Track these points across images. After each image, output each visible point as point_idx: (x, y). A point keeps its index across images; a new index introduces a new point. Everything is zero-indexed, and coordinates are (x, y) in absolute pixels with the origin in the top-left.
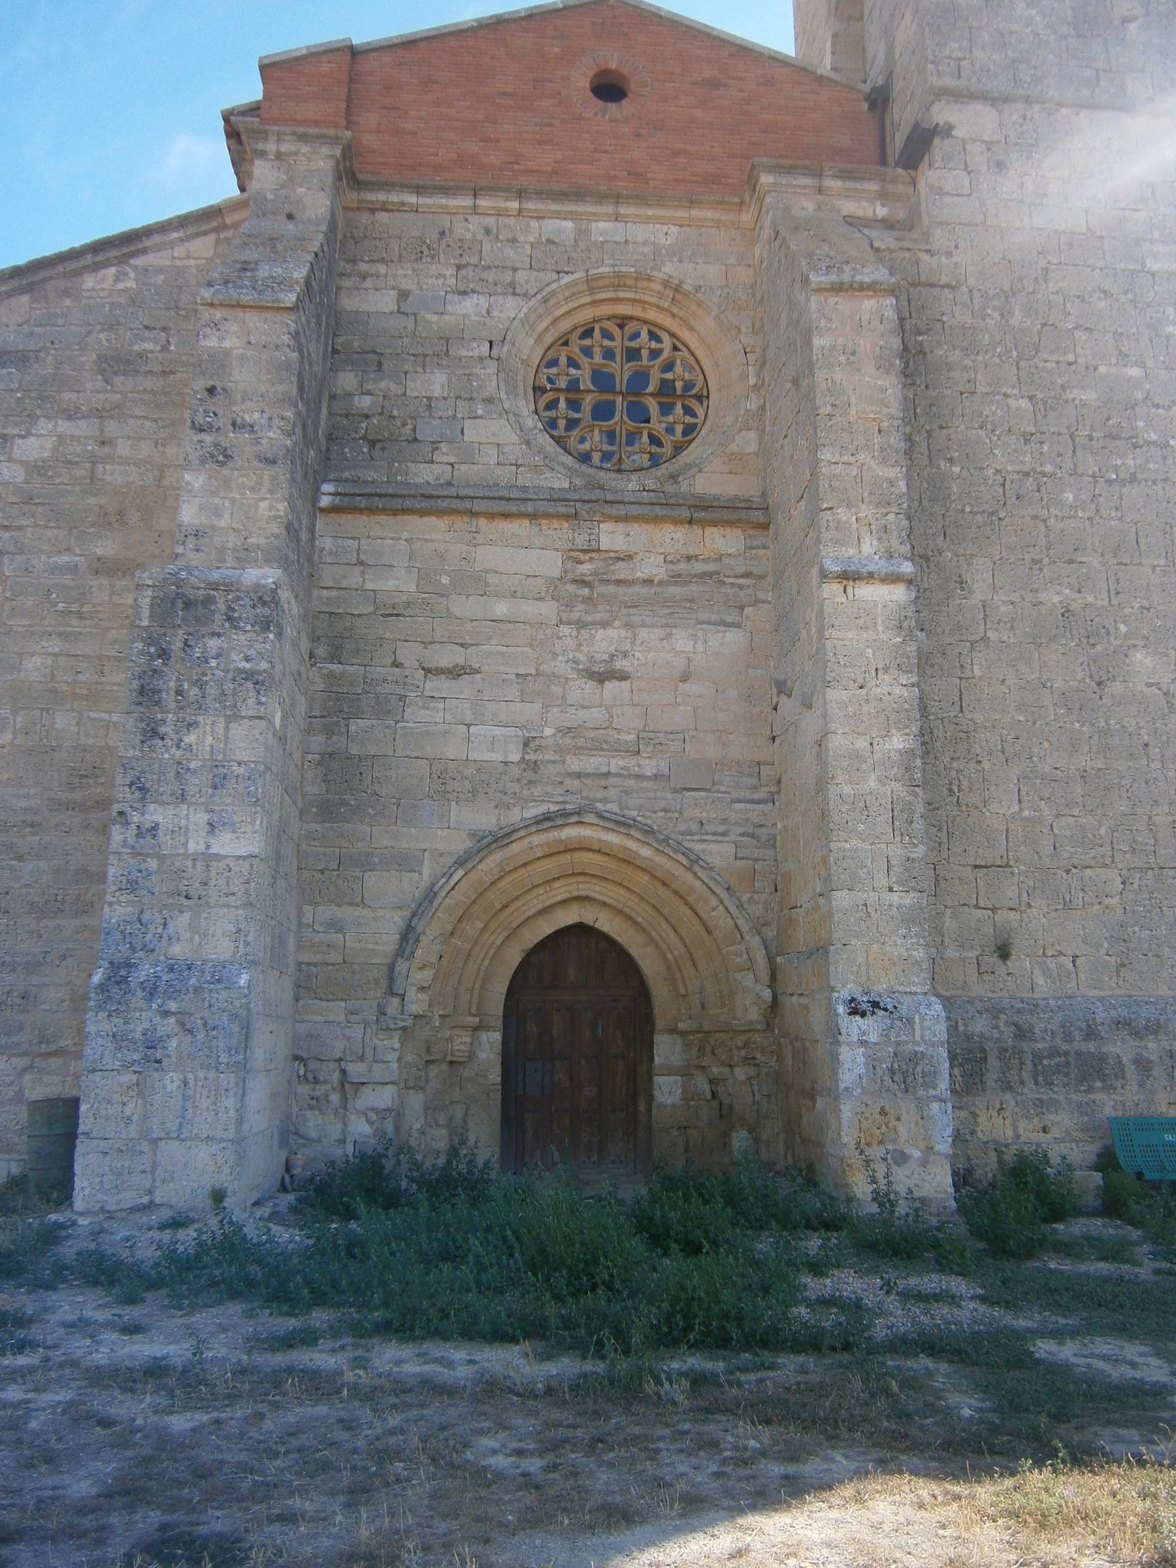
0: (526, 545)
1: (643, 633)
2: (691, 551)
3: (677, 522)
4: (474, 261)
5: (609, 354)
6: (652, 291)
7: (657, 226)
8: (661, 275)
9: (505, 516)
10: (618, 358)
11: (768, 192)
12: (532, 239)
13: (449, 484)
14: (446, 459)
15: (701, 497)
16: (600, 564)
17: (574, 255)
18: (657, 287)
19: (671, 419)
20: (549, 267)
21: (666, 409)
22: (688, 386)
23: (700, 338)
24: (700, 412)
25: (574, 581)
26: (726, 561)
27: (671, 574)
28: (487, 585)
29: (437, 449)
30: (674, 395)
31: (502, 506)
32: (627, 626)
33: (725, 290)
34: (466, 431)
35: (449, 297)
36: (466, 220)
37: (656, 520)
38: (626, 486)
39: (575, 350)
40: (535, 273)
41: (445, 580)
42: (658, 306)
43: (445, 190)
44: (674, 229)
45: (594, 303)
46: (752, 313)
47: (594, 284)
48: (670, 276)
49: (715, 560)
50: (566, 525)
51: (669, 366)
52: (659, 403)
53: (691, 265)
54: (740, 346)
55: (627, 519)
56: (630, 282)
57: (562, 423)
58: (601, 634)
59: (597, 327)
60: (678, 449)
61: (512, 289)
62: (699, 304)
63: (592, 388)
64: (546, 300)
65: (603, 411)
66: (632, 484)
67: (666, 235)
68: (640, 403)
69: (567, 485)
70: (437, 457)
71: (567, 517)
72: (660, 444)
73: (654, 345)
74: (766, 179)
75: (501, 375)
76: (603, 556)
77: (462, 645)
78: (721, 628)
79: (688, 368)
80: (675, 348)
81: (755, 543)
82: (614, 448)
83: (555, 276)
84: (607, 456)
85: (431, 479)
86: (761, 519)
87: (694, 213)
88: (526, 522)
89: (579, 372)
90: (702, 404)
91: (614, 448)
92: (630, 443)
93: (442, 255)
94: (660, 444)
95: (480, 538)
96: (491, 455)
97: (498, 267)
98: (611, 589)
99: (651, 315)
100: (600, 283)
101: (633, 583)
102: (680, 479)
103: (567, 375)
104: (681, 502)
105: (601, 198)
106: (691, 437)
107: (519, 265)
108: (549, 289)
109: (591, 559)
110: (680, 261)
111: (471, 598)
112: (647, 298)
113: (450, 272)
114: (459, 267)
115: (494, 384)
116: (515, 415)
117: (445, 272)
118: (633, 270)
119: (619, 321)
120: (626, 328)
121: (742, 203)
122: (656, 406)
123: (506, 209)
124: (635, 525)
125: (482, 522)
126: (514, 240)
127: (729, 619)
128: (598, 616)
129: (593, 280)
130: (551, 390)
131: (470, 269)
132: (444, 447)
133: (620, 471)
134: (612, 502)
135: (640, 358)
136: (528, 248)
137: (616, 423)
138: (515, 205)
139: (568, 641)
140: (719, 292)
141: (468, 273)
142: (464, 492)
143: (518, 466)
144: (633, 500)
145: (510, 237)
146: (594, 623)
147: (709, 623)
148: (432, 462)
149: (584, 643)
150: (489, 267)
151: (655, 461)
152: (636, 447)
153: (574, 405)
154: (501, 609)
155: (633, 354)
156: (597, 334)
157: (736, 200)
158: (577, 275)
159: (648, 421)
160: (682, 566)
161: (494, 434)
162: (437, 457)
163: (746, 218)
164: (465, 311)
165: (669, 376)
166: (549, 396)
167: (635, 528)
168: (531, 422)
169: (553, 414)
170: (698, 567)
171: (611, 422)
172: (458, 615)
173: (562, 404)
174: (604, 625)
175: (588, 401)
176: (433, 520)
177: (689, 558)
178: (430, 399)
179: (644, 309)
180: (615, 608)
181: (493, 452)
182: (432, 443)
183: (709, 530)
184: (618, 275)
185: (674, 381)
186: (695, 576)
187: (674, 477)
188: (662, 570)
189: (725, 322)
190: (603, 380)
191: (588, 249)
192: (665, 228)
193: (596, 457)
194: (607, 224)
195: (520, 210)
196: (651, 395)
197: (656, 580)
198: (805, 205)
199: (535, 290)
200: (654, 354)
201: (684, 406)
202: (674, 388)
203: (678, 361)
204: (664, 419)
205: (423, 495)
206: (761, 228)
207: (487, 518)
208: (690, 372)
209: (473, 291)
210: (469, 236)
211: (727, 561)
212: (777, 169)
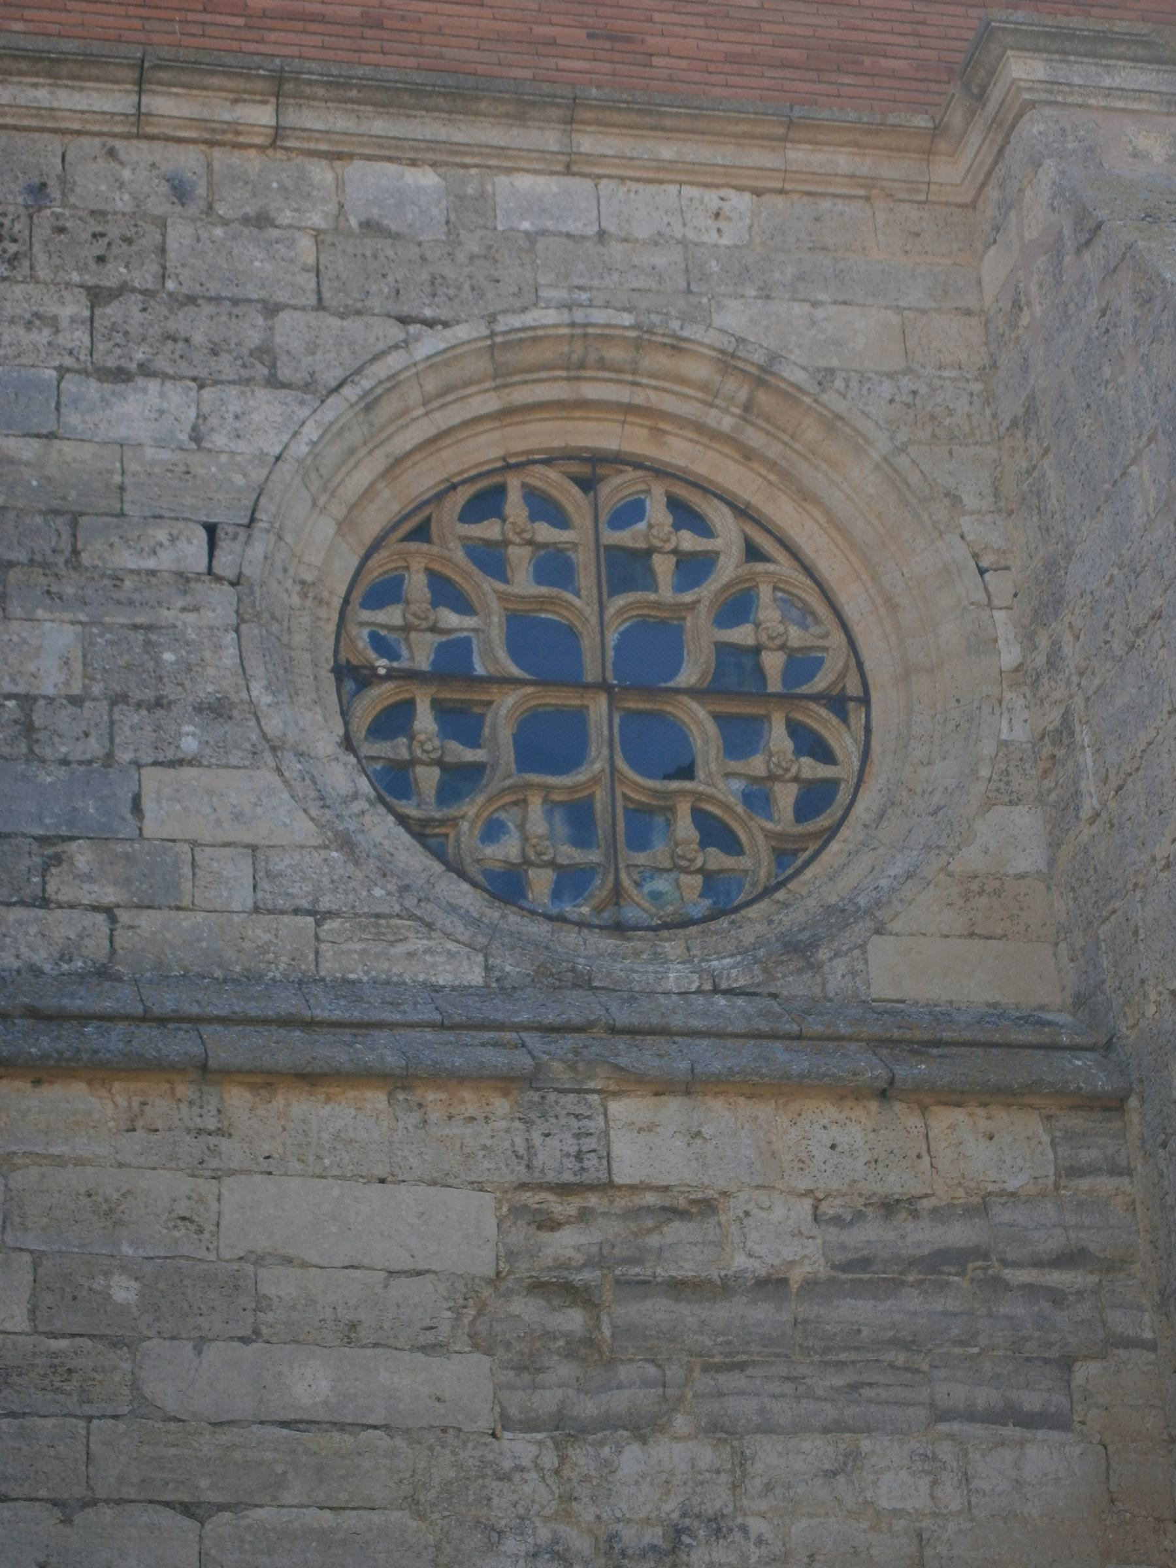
0: (380, 1171)
1: (769, 1456)
2: (895, 1182)
3: (846, 1092)
4: (143, 277)
5: (555, 567)
6: (683, 381)
7: (689, 191)
8: (711, 337)
9: (309, 1078)
10: (586, 579)
11: (1032, 104)
12: (316, 219)
13: (103, 973)
14: (88, 894)
15: (892, 1011)
16: (613, 1229)
17: (450, 272)
18: (699, 370)
19: (757, 765)
20: (375, 304)
21: (741, 736)
22: (802, 665)
23: (836, 525)
24: (845, 744)
25: (537, 1287)
26: (1002, 1214)
27: (839, 1258)
28: (262, 1303)
29: (58, 860)
30: (764, 696)
31: (292, 1048)
32: (717, 1430)
33: (906, 382)
34: (147, 804)
35: (70, 385)
36: (112, 153)
37: (785, 1088)
38: (661, 977)
39: (451, 547)
40: (334, 322)
41: (124, 1291)
42: (700, 428)
43: (49, 65)
44: (742, 202)
45: (506, 413)
46: (991, 452)
47: (511, 358)
48: (741, 340)
49: (970, 1211)
50: (501, 1105)
51: (737, 607)
52: (717, 717)
53: (799, 309)
54: (961, 552)
55: (690, 1086)
56: (617, 354)
57: (428, 778)
58: (631, 1458)
59: (514, 483)
60: (789, 856)
61: (266, 368)
62: (832, 423)
63: (516, 671)
64: (369, 404)
65: (550, 743)
66: (672, 972)
67: (723, 219)
68: (659, 716)
69: (476, 977)
70: (59, 886)
71: (506, 1082)
72: (731, 844)
73: (688, 541)
74: (1024, 69)
75: (251, 631)
76: (622, 1203)
77: (187, 1509)
78: (1011, 1432)
79: (788, 601)
80: (753, 553)
81: (1087, 1156)
82: (594, 856)
83: (396, 333)
84: (572, 881)
85: (41, 957)
86: (1102, 1083)
87: (798, 155)
88: (377, 1098)
89: (470, 622)
90: (844, 719)
91: (594, 856)
92: (639, 841)
93: (42, 258)
94: (731, 844)
95: (232, 1151)
96: (234, 882)
97: (216, 300)
98: (656, 1311)
99: (679, 451)
100: (531, 356)
101: (724, 1288)
102: (823, 954)
103: (433, 629)
104: (844, 1029)
105: (523, 105)
106: (823, 821)
107: (282, 296)
108: (380, 370)
109: (585, 1216)
110: (766, 296)
111: (212, 1352)
112: (669, 403)
113: (73, 308)
114: (97, 296)
115: (229, 658)
116: (300, 755)
117: (53, 309)
118: (627, 319)
119: (575, 468)
120: (604, 490)
121: (938, 130)
122: (711, 728)
123: (235, 127)
124: (718, 1105)
125: (237, 1098)
126: (262, 221)
127: (1031, 1402)
128: (619, 1401)
129: (507, 345)
130: (391, 675)
131: (133, 302)
132: (82, 856)
133: (619, 928)
134: (632, 1031)
135: (648, 581)
136: (306, 243)
137: (595, 780)
138: (262, 115)
139: (531, 1486)
140: (887, 389)
141: (123, 312)
142: (167, 1001)
143: (321, 917)
144: (697, 1023)
145: (250, 210)
146: (608, 1423)
147: (971, 1416)
148: (44, 902)
149: (583, 1491)
150: (191, 300)
151: (723, 898)
152: (659, 853)
153: (460, 721)
154: (311, 1383)
155: (626, 569)
156: (515, 506)
157: (921, 121)
158: (461, 332)
159: (687, 772)
160: (870, 1234)
161: (238, 816)
162: (59, 886)
163: (951, 172)
164: (122, 431)
165: (742, 635)
166: (380, 696)
167: (720, 1115)
168: (342, 776)
169: (399, 749)
170: (922, 1237)
171: (580, 776)
172: (171, 1407)
173: (425, 721)
174: (642, 1428)
175: (506, 709)
176: (74, 1096)
177: (889, 1207)
178: (27, 701)
179: (656, 432)
180: (674, 1372)
181: (240, 871)
182: (43, 840)
183: (944, 1119)
184: (583, 334)
185: (757, 650)
186: (913, 1263)
187: (799, 949)
188: (813, 1248)
189: (914, 478)
190: (543, 645)
191: (489, 255)
192: (712, 197)
193: (541, 882)
194: (541, 180)
195: (279, 132)
196: (692, 692)
197: (796, 1277)
198: (1142, 143)
199: (340, 373)
200: (692, 568)
201: (795, 730)
202: (759, 672)
203: (765, 592)
204: (736, 766)
205: (33, 1013)
206: (1006, 206)
207: (254, 1087)
208: (804, 626)
209: (145, 370)
210: (122, 202)
211: (1006, 1216)
212: (1057, 43)
